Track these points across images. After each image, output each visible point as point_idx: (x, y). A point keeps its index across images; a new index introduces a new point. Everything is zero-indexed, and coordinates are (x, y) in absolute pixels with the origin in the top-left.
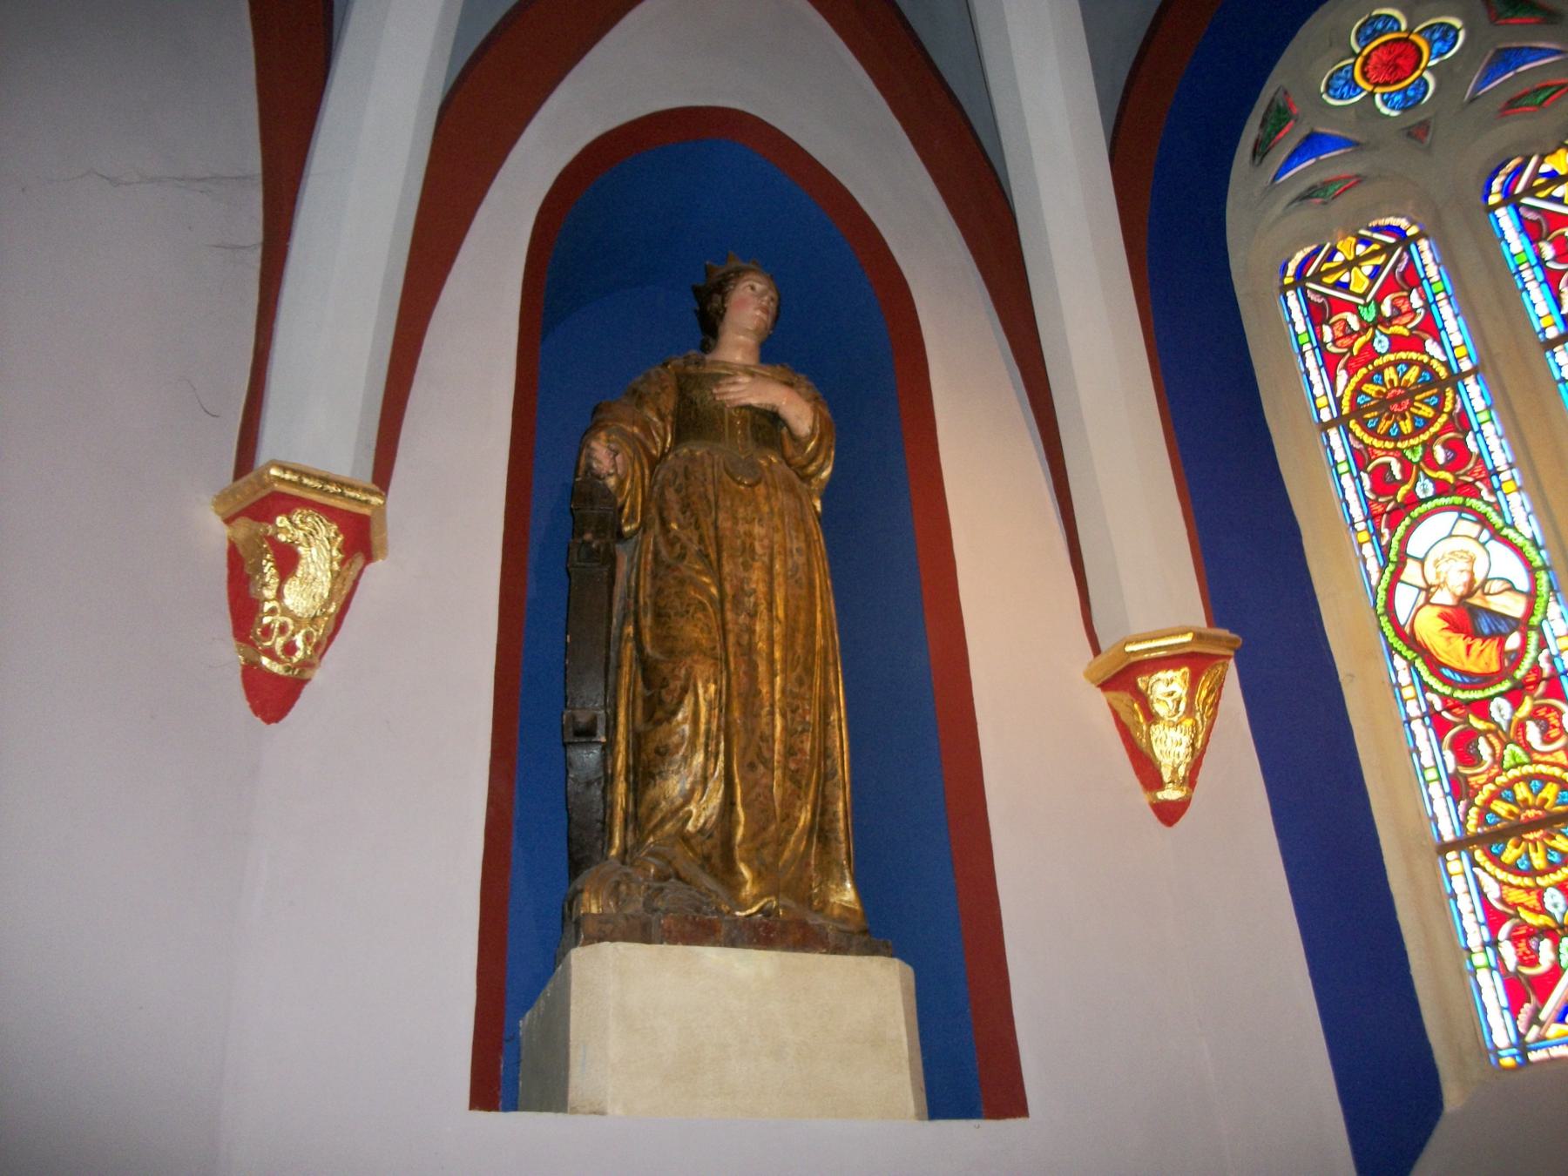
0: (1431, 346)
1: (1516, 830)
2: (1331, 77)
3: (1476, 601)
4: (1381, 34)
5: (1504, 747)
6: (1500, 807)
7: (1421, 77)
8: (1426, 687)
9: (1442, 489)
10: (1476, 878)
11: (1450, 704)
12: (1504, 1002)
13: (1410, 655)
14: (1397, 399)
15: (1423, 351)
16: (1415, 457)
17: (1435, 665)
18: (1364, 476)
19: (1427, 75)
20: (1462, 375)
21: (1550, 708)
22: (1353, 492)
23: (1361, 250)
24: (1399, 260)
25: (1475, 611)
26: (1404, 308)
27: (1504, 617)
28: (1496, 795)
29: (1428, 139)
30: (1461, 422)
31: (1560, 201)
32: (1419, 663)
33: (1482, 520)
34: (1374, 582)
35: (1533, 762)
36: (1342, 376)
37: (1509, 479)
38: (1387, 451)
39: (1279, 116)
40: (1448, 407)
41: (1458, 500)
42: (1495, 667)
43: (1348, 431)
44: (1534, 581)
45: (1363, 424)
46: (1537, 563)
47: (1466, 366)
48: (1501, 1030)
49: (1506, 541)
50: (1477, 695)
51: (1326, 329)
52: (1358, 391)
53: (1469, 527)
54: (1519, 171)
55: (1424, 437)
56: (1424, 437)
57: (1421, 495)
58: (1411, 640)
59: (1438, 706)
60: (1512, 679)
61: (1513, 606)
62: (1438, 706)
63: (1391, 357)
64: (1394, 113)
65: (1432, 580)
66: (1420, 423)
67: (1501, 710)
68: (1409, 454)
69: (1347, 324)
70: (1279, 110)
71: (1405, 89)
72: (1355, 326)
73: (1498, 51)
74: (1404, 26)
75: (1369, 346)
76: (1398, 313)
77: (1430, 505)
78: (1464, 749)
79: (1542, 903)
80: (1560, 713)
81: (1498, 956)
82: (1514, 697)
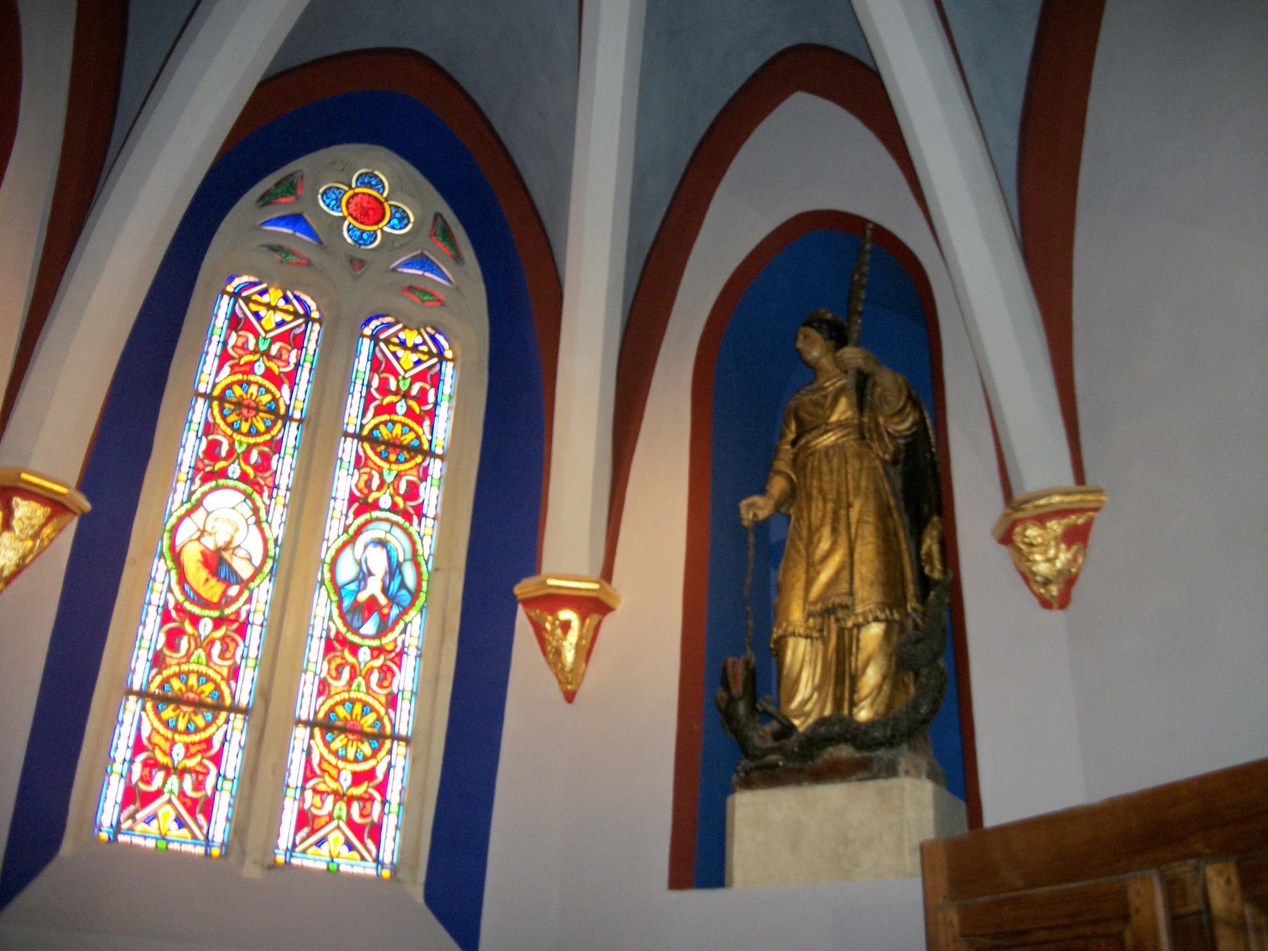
0: (285, 388)
1: (178, 701)
2: (330, 188)
3: (226, 555)
4: (371, 187)
5: (196, 648)
6: (176, 684)
7: (375, 232)
8: (170, 590)
9: (244, 477)
10: (140, 719)
11: (179, 608)
12: (119, 799)
13: (170, 564)
14: (249, 407)
15: (279, 388)
16: (240, 449)
17: (182, 579)
18: (204, 441)
19: (379, 233)
20: (292, 419)
21: (233, 640)
22: (191, 448)
23: (281, 303)
24: (299, 326)
25: (222, 561)
26: (285, 357)
27: (236, 574)
28: (177, 675)
29: (359, 273)
30: (276, 445)
31: (398, 359)
32: (174, 573)
33: (256, 511)
34: (174, 508)
35: (367, 693)
36: (226, 369)
37: (282, 495)
38: (225, 435)
39: (290, 186)
40: (274, 432)
41: (249, 490)
42: (215, 600)
43: (210, 406)
44: (263, 563)
45: (222, 409)
46: (271, 553)
47: (297, 415)
48: (108, 814)
49: (262, 531)
50: (196, 610)
51: (234, 335)
52: (229, 386)
53: (246, 509)
54: (389, 326)
55: (252, 440)
56: (252, 440)
57: (230, 474)
58: (177, 557)
59: (171, 605)
60: (222, 612)
61: (245, 571)
62: (171, 605)
63: (261, 380)
64: (349, 240)
65: (208, 528)
66: (253, 431)
67: (206, 626)
68: (237, 444)
69: (247, 341)
70: (291, 183)
71: (363, 232)
72: (251, 347)
73: (422, 255)
74: (385, 195)
75: (252, 364)
76: (279, 357)
77: (230, 483)
78: (173, 638)
79: (171, 750)
80: (393, 675)
81: (130, 771)
82: (218, 623)
